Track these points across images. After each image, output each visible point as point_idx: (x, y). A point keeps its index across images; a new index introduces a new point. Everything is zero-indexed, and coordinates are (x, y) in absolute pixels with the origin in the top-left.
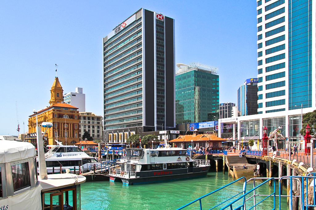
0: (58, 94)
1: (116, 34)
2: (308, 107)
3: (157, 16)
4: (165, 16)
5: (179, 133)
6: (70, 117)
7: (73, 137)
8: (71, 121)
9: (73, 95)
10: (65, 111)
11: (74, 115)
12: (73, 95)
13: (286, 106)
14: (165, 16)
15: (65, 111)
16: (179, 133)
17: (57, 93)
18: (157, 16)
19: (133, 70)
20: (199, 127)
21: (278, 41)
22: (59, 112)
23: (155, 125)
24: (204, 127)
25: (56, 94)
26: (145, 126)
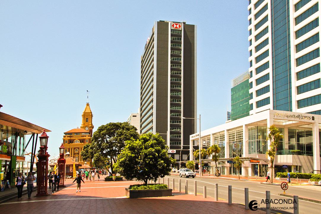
2: (167, 135)
5: (175, 152)
6: (82, 142)
9: (133, 116)
10: (77, 136)
11: (85, 139)
12: (133, 116)
15: (77, 136)
16: (175, 152)
17: (87, 118)
18: (173, 26)
21: (315, 57)
25: (85, 119)
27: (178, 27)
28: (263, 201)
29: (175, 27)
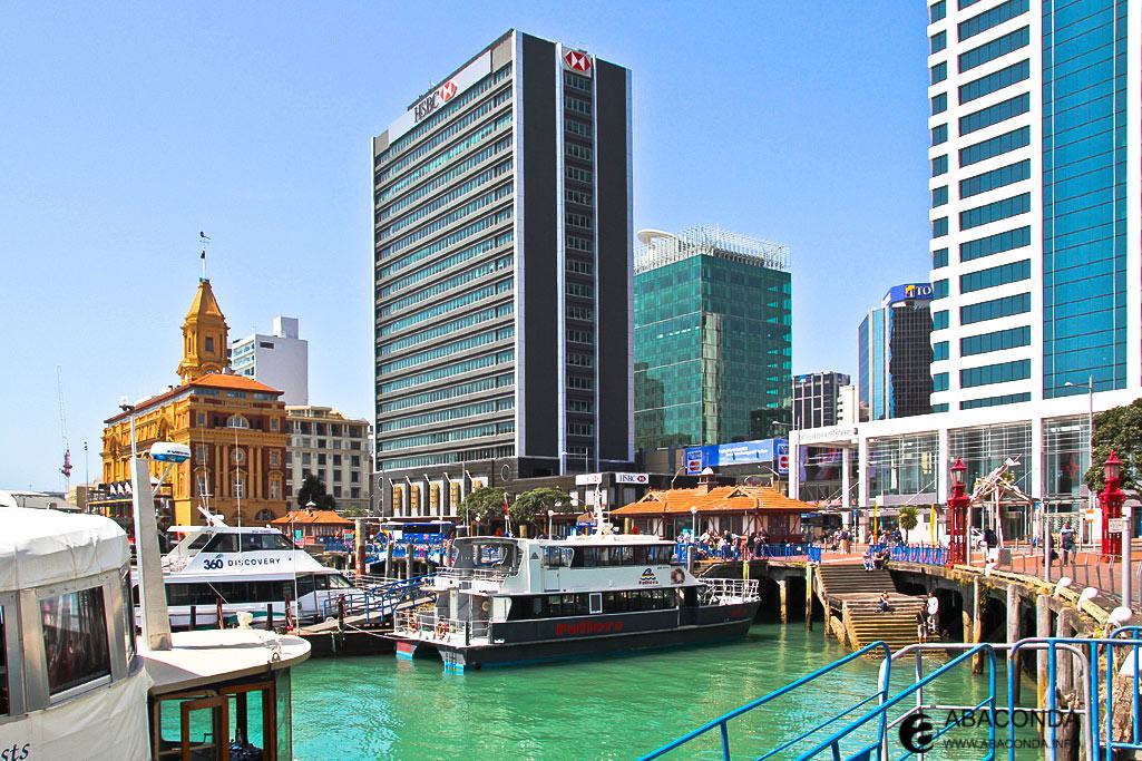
0: (209, 339)
1: (420, 121)
3: (569, 58)
4: (597, 60)
5: (647, 482)
7: (265, 495)
8: (258, 439)
9: (263, 345)
10: (237, 403)
11: (268, 417)
12: (263, 345)
13: (1034, 384)
14: (597, 60)
16: (647, 482)
18: (569, 58)
19: (480, 256)
20: (717, 461)
22: (211, 407)
23: (562, 454)
24: (738, 461)
25: (203, 340)
26: (524, 456)
27: (573, 56)
28: (952, 718)
29: (574, 64)
